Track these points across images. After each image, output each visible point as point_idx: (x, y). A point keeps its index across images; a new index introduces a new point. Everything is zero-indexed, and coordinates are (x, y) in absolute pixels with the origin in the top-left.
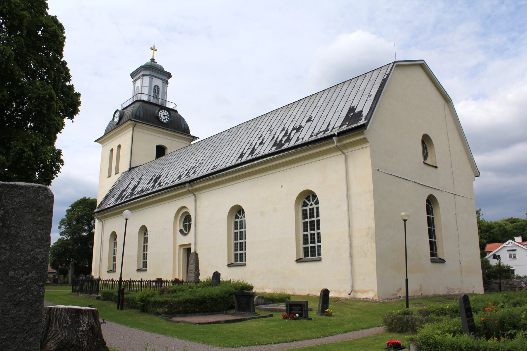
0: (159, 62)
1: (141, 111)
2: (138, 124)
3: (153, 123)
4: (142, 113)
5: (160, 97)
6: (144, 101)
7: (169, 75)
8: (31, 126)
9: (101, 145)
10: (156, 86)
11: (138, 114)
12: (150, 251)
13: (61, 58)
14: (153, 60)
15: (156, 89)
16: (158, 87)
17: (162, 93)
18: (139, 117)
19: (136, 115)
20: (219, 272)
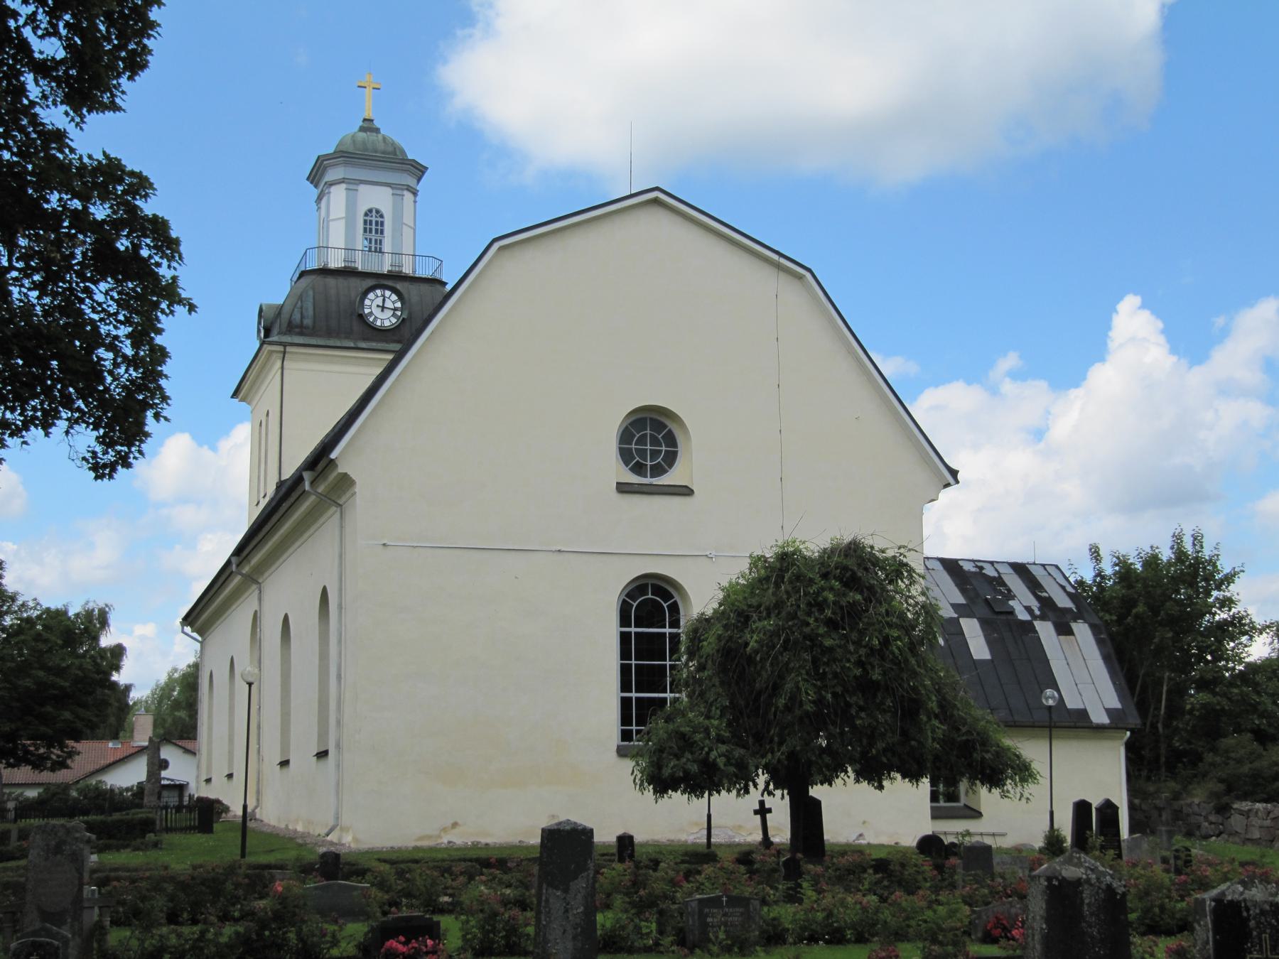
0: (390, 130)
1: (309, 305)
2: (289, 349)
3: (349, 335)
4: (311, 312)
5: (387, 247)
6: (325, 272)
7: (419, 170)
8: (86, 236)
9: (249, 408)
10: (370, 211)
11: (297, 317)
12: (248, 844)
13: (88, 85)
14: (368, 126)
15: (374, 223)
16: (378, 211)
17: (394, 230)
18: (301, 326)
19: (290, 323)
20: (1077, 799)
